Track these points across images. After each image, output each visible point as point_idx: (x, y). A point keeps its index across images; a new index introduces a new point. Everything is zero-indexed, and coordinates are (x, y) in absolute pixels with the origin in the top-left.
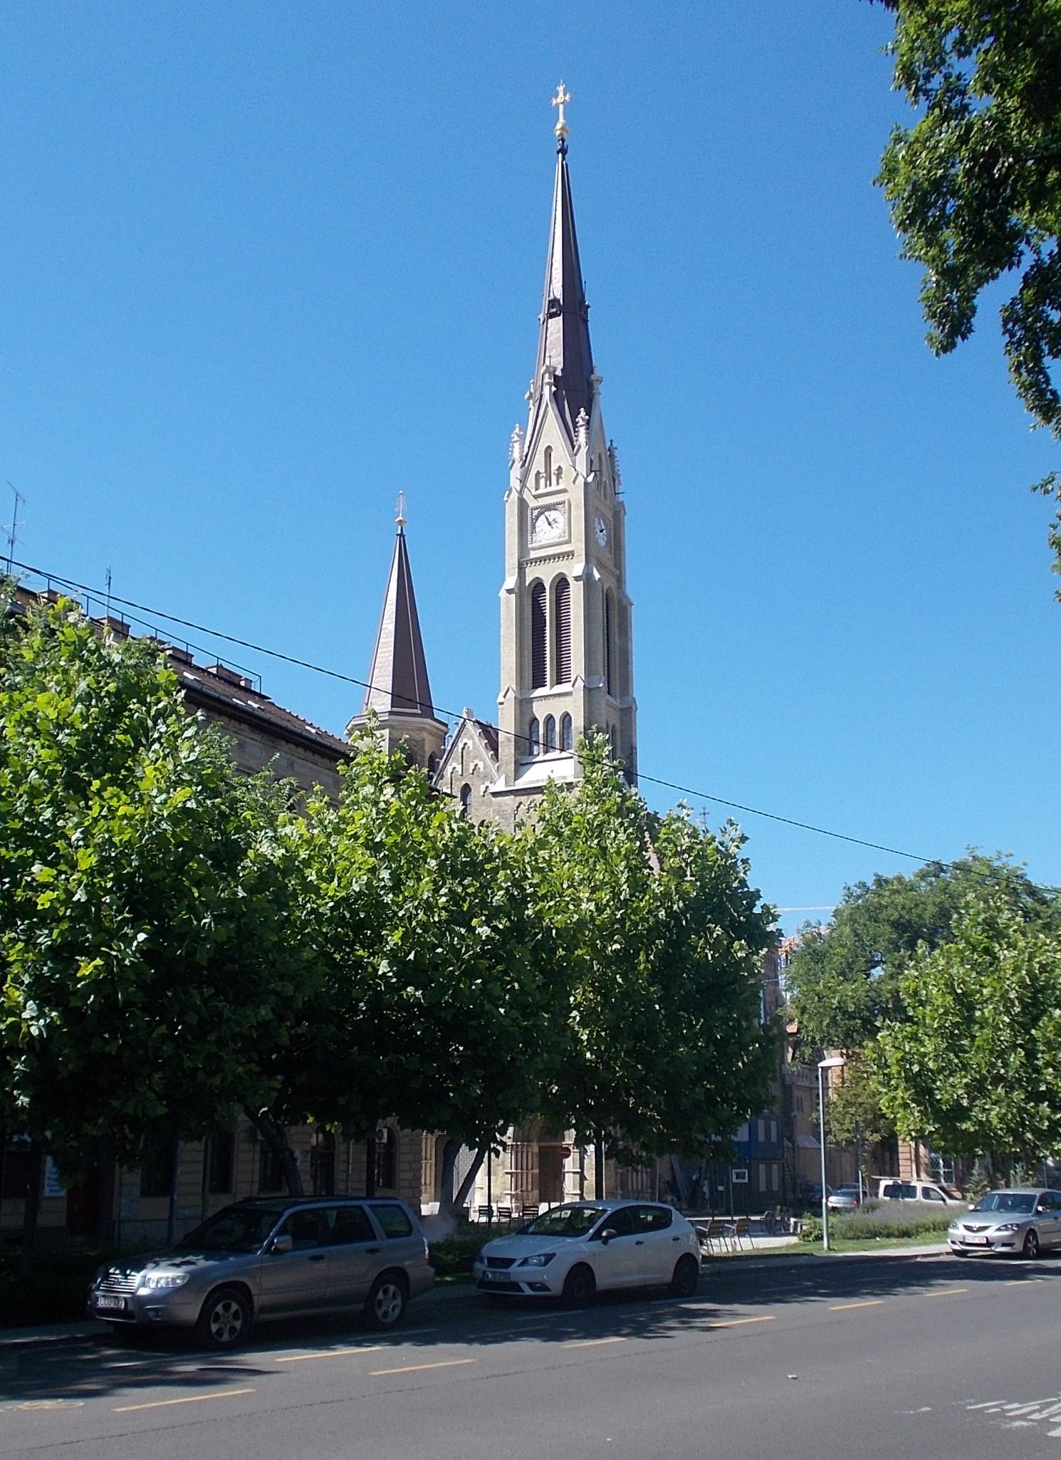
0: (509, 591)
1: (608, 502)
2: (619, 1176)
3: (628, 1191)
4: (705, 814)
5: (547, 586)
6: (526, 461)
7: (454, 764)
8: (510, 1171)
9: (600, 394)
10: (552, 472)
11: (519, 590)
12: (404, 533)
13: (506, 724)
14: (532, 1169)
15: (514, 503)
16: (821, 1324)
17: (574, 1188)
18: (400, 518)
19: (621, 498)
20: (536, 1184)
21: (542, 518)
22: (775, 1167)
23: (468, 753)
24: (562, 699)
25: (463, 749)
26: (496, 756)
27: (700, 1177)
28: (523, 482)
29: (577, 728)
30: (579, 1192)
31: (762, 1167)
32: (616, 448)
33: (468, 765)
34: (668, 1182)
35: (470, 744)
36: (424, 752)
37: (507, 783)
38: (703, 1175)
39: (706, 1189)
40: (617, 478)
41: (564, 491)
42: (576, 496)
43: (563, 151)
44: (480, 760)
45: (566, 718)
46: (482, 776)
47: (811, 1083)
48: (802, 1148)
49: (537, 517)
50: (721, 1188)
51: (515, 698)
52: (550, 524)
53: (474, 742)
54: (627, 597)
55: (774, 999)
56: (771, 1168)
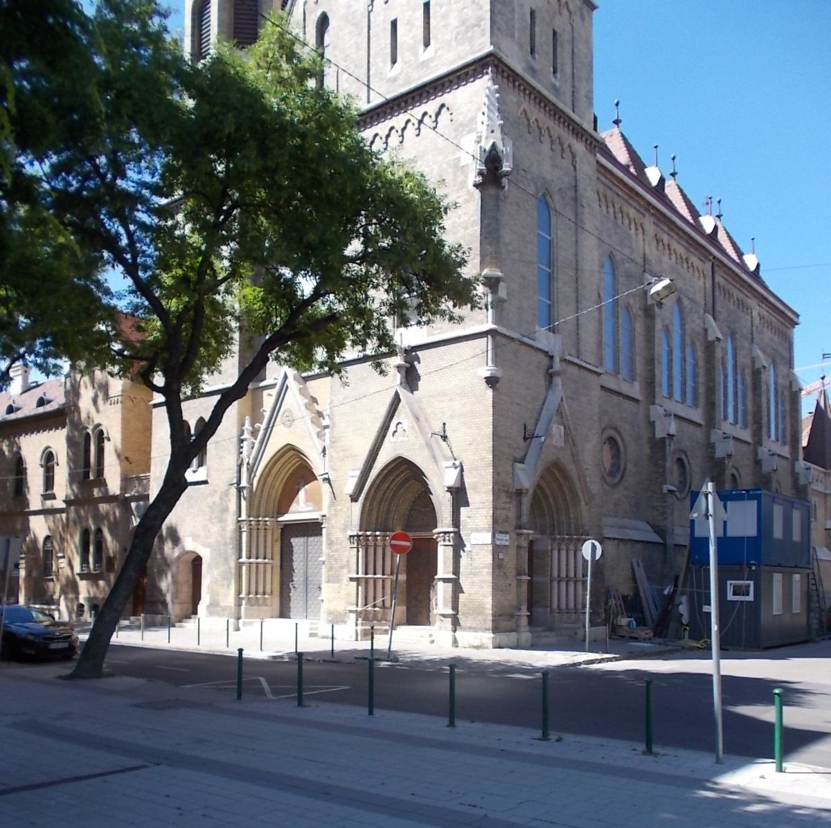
16: (664, 513)
17: (445, 605)
22: (797, 577)
27: (675, 591)
30: (450, 612)
31: (777, 578)
34: (624, 598)
38: (679, 589)
39: (683, 609)
47: (826, 489)
55: (788, 384)
56: (791, 579)
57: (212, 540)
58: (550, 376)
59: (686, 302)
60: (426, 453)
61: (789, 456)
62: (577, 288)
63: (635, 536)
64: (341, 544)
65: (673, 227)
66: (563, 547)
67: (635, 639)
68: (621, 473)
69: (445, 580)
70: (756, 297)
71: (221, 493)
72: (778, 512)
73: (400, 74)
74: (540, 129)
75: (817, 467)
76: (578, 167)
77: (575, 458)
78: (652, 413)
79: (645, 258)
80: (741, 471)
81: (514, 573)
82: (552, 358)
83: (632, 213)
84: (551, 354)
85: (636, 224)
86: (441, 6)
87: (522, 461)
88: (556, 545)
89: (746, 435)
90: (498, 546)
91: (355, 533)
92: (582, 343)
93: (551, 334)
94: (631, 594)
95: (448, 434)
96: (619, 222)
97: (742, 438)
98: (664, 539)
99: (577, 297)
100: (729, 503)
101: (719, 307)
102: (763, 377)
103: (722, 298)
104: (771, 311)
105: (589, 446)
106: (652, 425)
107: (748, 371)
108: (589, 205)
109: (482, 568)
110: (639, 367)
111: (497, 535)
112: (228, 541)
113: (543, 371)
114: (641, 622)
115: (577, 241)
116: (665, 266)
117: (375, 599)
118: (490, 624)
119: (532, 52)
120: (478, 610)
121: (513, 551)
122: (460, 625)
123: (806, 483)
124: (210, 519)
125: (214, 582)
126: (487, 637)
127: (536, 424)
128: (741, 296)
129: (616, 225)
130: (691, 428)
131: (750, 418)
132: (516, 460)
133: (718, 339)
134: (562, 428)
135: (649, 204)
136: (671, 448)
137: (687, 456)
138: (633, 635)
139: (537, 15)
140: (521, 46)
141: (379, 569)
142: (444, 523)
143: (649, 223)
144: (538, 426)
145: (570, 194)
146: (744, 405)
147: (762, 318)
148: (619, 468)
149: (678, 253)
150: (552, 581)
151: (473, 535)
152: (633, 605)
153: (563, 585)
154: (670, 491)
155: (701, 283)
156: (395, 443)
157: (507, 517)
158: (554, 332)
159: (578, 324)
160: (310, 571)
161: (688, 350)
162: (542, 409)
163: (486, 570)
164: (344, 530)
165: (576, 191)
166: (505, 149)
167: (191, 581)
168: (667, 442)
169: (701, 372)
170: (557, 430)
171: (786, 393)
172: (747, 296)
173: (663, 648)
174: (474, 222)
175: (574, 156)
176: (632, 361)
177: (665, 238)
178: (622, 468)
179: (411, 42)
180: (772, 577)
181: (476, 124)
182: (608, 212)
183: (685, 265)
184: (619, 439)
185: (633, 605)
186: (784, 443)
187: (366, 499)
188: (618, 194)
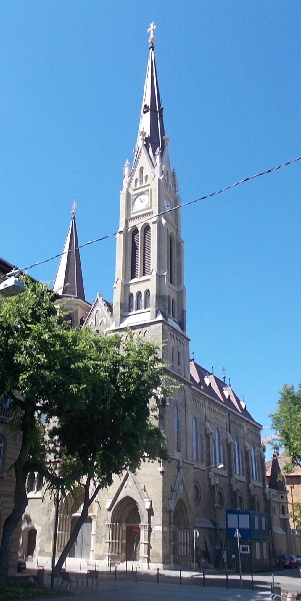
0: (121, 232)
1: (172, 194)
2: (172, 547)
3: (178, 556)
4: (224, 370)
5: (139, 230)
6: (131, 175)
7: (92, 321)
8: (108, 541)
9: (183, 242)
10: (143, 178)
11: (125, 233)
12: (75, 217)
13: (117, 299)
14: (122, 540)
15: (124, 193)
16: (215, 516)
17: (145, 553)
18: (74, 211)
19: (178, 194)
20: (124, 549)
21: (138, 199)
22: (265, 544)
23: (99, 315)
24: (146, 283)
25: (96, 313)
26: (112, 315)
28: (129, 185)
29: (152, 295)
30: (147, 556)
31: (257, 544)
32: (176, 172)
33: (98, 320)
34: (203, 551)
35: (100, 310)
36: (78, 316)
37: (116, 326)
38: (223, 549)
39: (224, 556)
40: (176, 185)
41: (149, 185)
42: (154, 186)
43: (153, 48)
44: (104, 318)
45: (148, 292)
46: (105, 325)
48: (276, 533)
49: (135, 199)
50: (233, 556)
51: (122, 283)
52: (142, 201)
53: (102, 309)
54: (181, 239)
55: (259, 455)
57: (43, 523)
59: (220, 429)
60: (138, 495)
61: (262, 486)
62: (186, 435)
63: (205, 525)
64: (102, 527)
65: (215, 403)
66: (182, 531)
67: (208, 568)
68: (199, 500)
69: (94, 535)
70: (245, 422)
71: (49, 503)
72: (256, 518)
75: (274, 490)
77: (187, 498)
78: (210, 475)
79: (206, 416)
80: (243, 495)
81: (168, 541)
82: (179, 462)
83: (201, 401)
84: (179, 460)
85: (202, 405)
87: (171, 500)
88: (180, 531)
89: (244, 479)
91: (109, 524)
93: (178, 452)
94: (205, 550)
95: (146, 489)
96: (197, 405)
97: (242, 480)
98: (215, 526)
99: (186, 438)
100: (239, 515)
101: (231, 429)
102: (249, 454)
103: (233, 425)
104: (251, 426)
106: (210, 480)
107: (243, 452)
108: (189, 406)
110: (205, 457)
112: (51, 524)
113: (176, 467)
114: (209, 561)
116: (212, 417)
117: (115, 550)
118: (162, 561)
120: (157, 555)
121: (168, 533)
122: (150, 561)
123: (270, 499)
124: (43, 514)
125: (42, 541)
126: (161, 566)
127: (175, 485)
128: (239, 422)
129: (196, 407)
130: (223, 478)
131: (245, 471)
132: (169, 499)
133: (232, 443)
135: (206, 397)
136: (217, 489)
137: (222, 490)
138: (207, 567)
139: (174, 349)
140: (170, 360)
141: (117, 538)
142: (144, 522)
143: (207, 404)
144: (175, 486)
145: (184, 403)
146: (243, 466)
147: (248, 429)
148: (198, 497)
149: (216, 411)
150: (178, 544)
151: (156, 527)
152: (206, 554)
153: (182, 546)
154: (217, 507)
155: (225, 421)
156: (126, 491)
157: (167, 520)
158: (179, 452)
160: (84, 538)
161: (221, 447)
162: (176, 480)
164: (104, 522)
167: (28, 540)
169: (226, 455)
170: (181, 487)
171: (259, 459)
172: (242, 422)
173: (218, 572)
176: (202, 455)
178: (200, 497)
180: (255, 544)
184: (199, 487)
185: (206, 554)
186: (259, 481)
187: (114, 511)
188: (197, 396)
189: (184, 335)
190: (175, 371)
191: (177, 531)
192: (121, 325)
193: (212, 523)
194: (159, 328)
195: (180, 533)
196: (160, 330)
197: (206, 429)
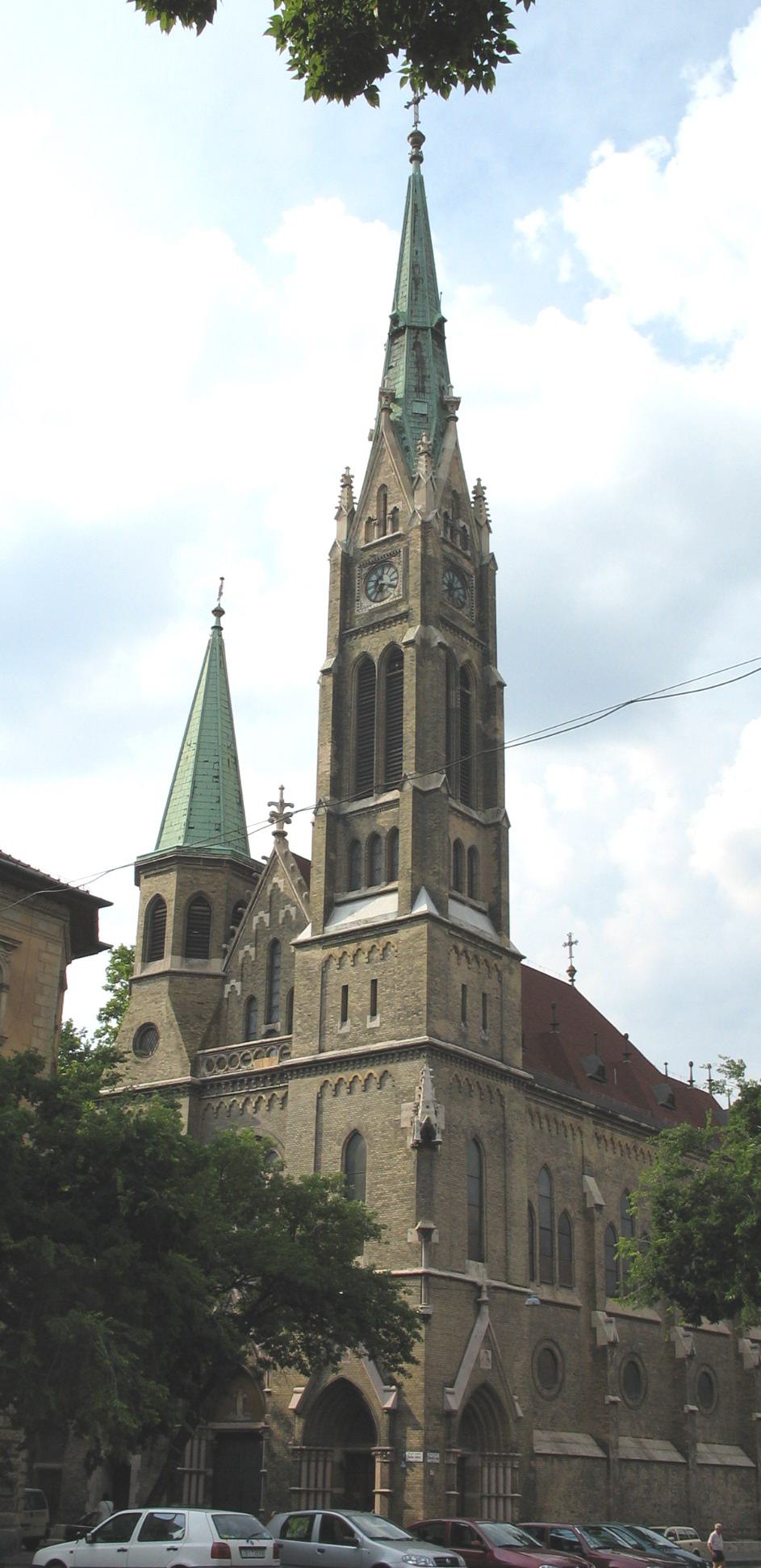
46: (293, 926)
58: (479, 1305)
73: (350, 1033)
74: (470, 1085)
76: (506, 1106)
86: (387, 987)
90: (429, 1463)
92: (512, 1267)
96: (554, 1133)
105: (518, 1365)
106: (593, 1330)
109: (416, 1484)
111: (428, 1454)
115: (505, 1174)
119: (464, 1018)
134: (489, 1352)
149: (624, 1144)
150: (482, 1497)
154: (614, 1403)
159: (507, 1251)
163: (418, 1486)
165: (505, 1128)
166: (439, 1122)
168: (609, 1350)
174: (411, 1177)
175: (502, 1097)
177: (608, 1133)
179: (360, 1009)
181: (414, 1095)
182: (541, 1128)
183: (633, 1154)
184: (557, 1352)
189: (502, 945)
190: (177, 1078)
191: (480, 1465)
192: (326, 928)
193: (599, 1445)
194: (418, 935)
195: (486, 1470)
196: (421, 942)
197: (585, 1195)
